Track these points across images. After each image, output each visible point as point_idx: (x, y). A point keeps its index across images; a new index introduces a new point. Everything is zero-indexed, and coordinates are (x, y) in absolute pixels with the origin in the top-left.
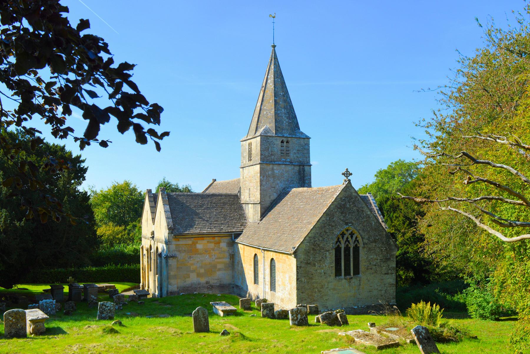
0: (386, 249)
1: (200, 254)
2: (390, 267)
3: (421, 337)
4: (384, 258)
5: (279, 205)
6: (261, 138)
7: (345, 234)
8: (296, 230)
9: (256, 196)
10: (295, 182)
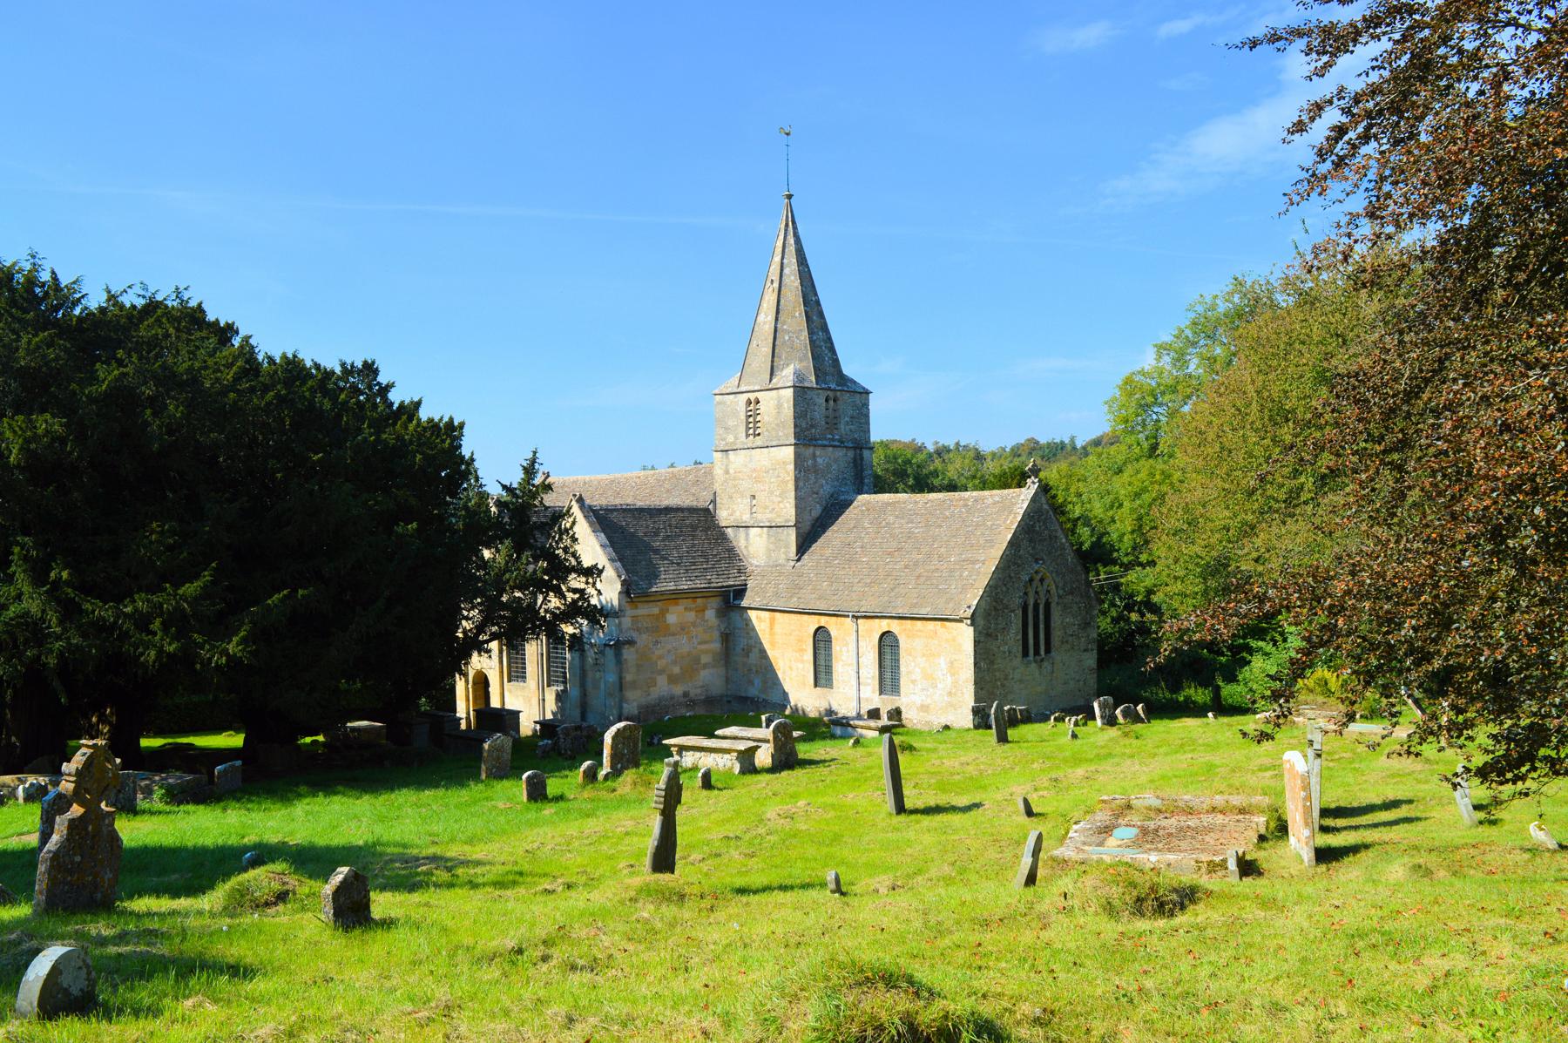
5: (834, 527)
6: (794, 392)
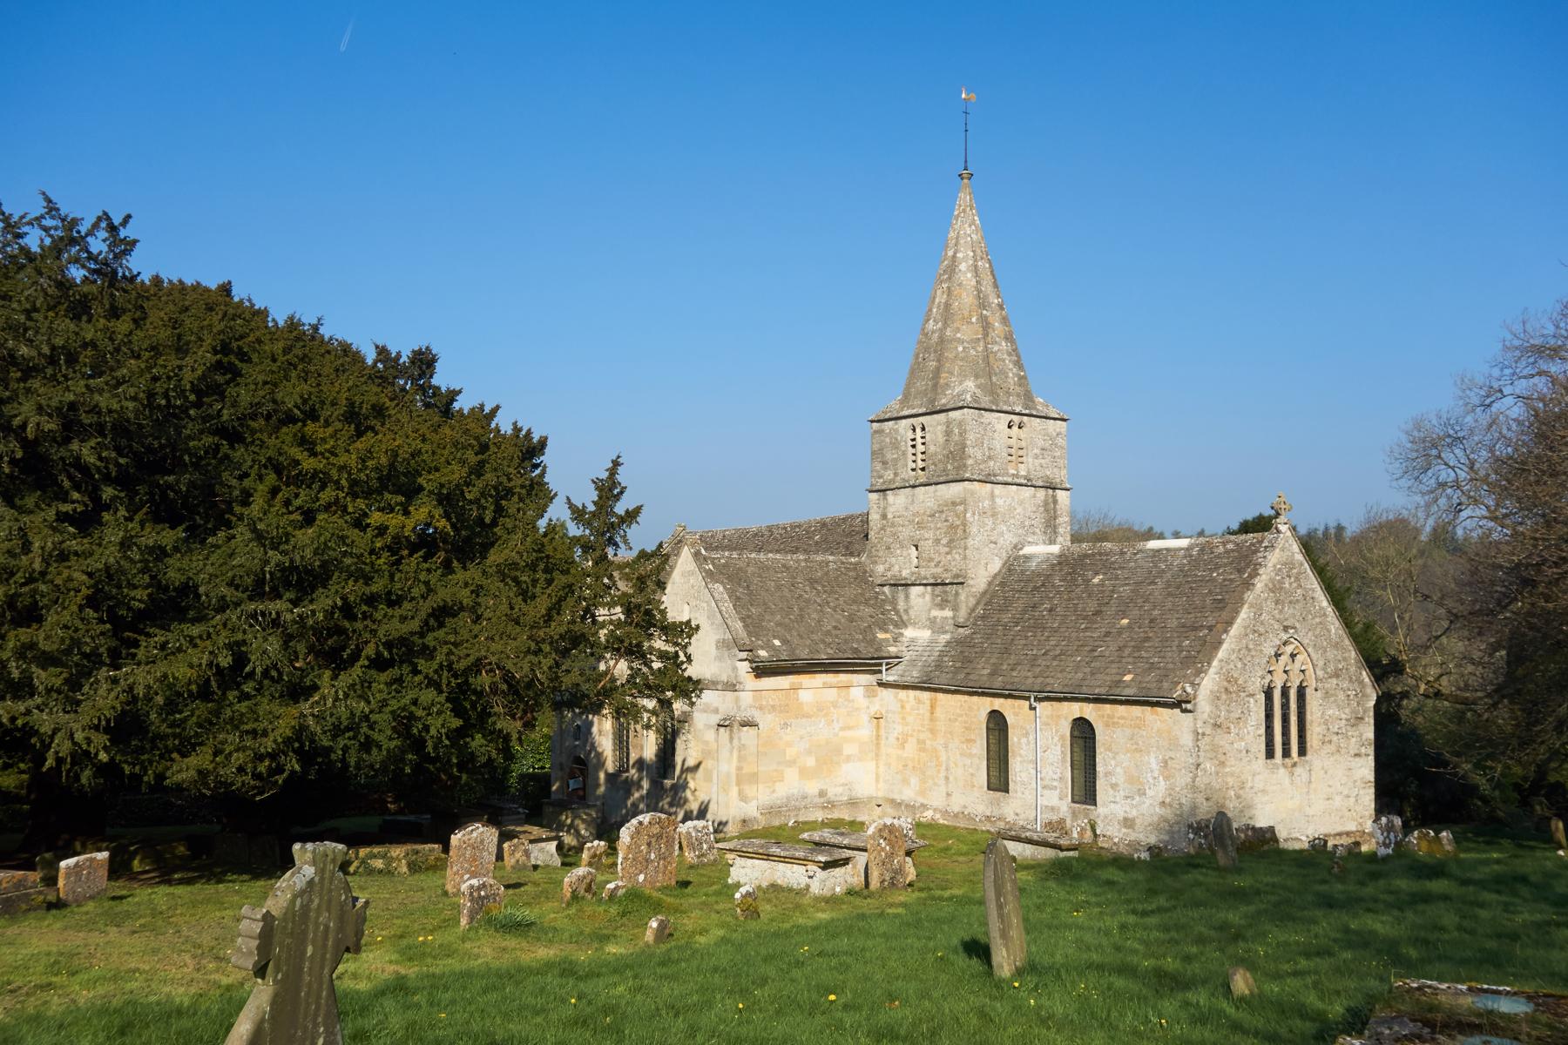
1: (807, 717)
4: (1354, 715)
10: (1038, 530)
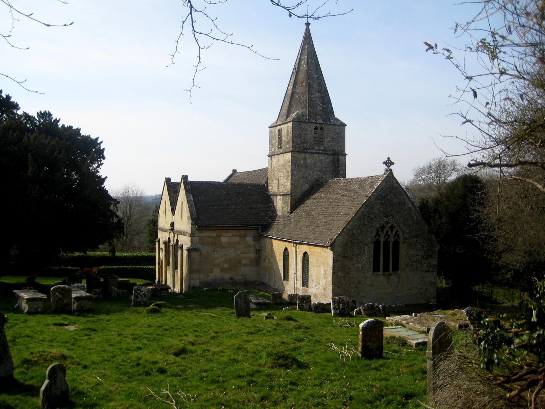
0: (428, 245)
2: (432, 264)
3: (472, 318)
7: (385, 227)
8: (332, 222)
9: (286, 186)
10: (329, 173)
